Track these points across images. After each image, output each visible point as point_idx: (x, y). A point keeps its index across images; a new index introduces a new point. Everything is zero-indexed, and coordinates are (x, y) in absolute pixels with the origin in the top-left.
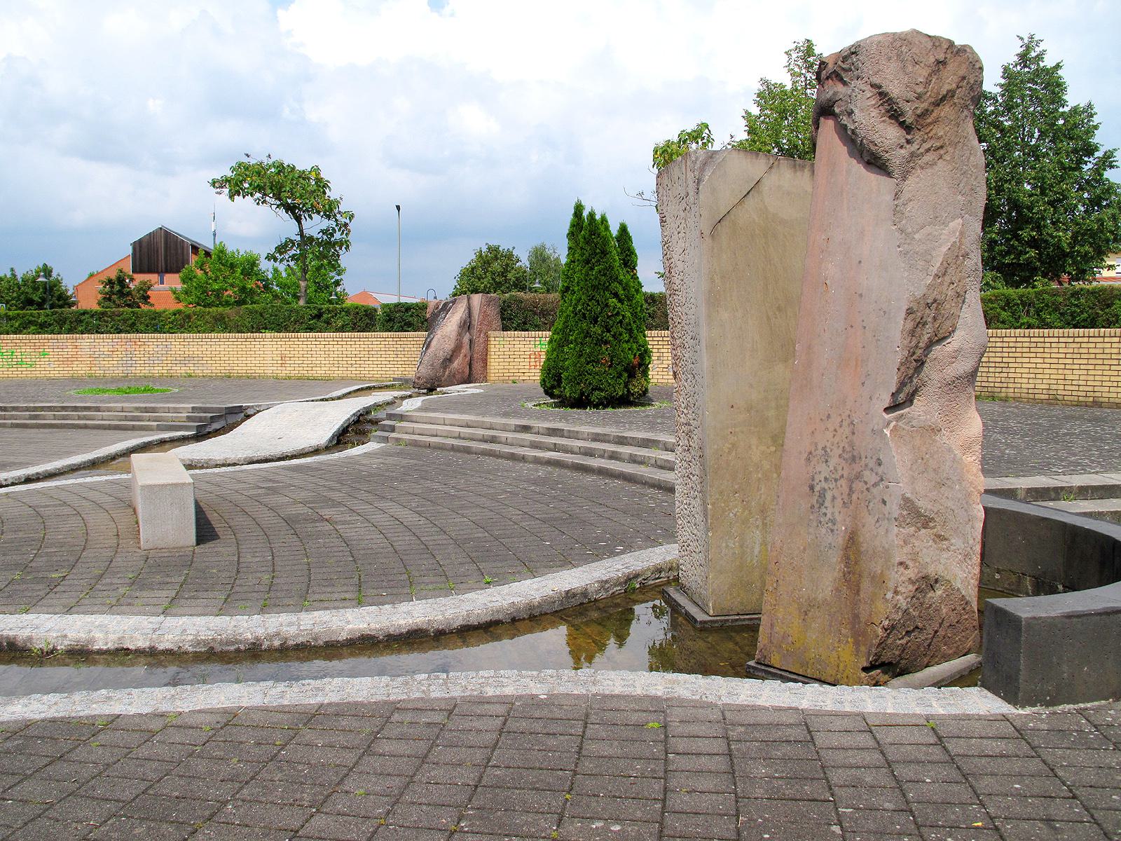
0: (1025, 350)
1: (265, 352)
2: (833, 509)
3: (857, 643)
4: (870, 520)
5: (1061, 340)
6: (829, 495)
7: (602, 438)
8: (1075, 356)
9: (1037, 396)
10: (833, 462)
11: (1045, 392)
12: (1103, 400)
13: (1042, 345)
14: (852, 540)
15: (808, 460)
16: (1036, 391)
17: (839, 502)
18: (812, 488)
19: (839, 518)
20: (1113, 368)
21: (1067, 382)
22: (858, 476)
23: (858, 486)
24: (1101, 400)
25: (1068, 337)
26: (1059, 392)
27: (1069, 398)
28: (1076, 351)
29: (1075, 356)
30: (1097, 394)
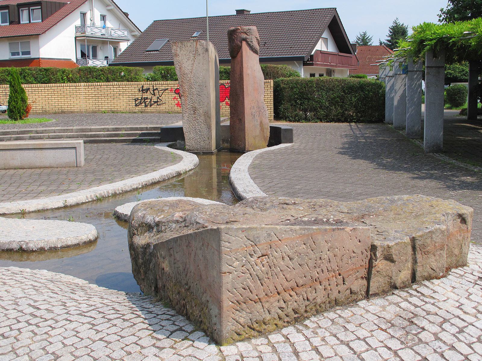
0: (30, 93)
1: (85, 94)
2: (257, 118)
3: (265, 141)
4: (264, 118)
5: (46, 88)
6: (255, 115)
7: (13, 133)
8: (52, 94)
9: (37, 111)
10: (255, 108)
11: (41, 109)
12: (66, 111)
13: (37, 91)
14: (261, 123)
15: (250, 109)
16: (37, 109)
17: (257, 116)
18: (252, 114)
19: (258, 119)
20: (68, 98)
21: (50, 105)
22: (260, 111)
23: (261, 113)
24: (65, 111)
25: (48, 87)
26: (47, 109)
27: (51, 111)
28: (52, 92)
29: (52, 94)
30: (63, 109)
